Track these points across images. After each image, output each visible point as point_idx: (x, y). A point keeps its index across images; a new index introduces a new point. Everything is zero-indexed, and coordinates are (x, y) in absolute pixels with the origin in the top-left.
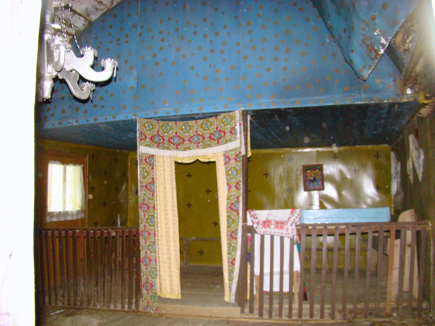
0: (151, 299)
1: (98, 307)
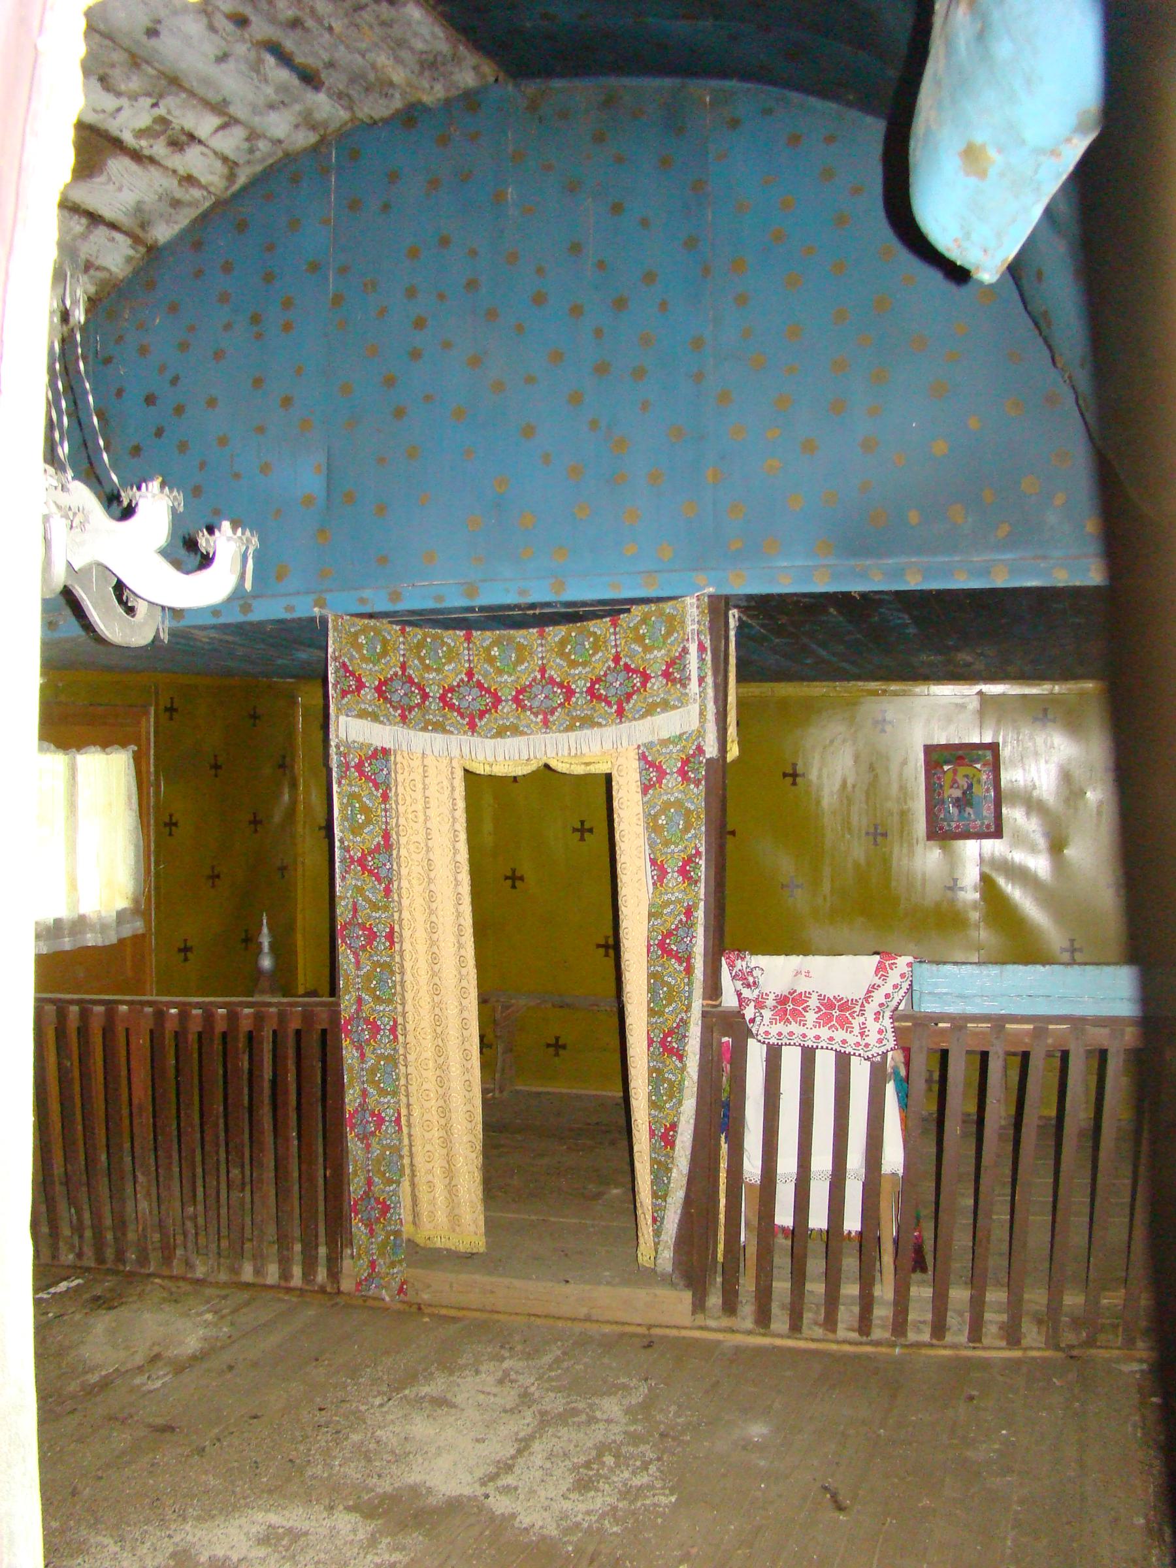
0: (382, 1254)
1: (200, 1271)
